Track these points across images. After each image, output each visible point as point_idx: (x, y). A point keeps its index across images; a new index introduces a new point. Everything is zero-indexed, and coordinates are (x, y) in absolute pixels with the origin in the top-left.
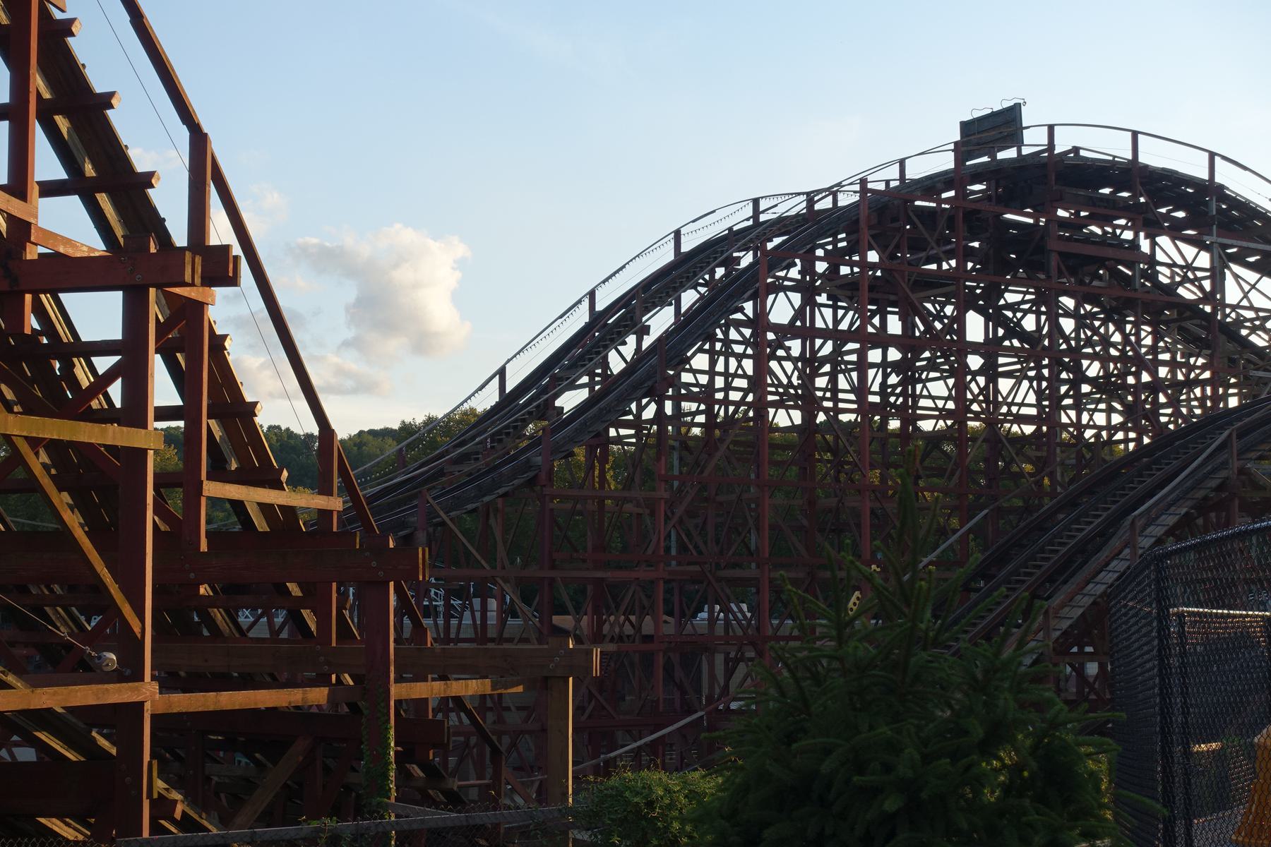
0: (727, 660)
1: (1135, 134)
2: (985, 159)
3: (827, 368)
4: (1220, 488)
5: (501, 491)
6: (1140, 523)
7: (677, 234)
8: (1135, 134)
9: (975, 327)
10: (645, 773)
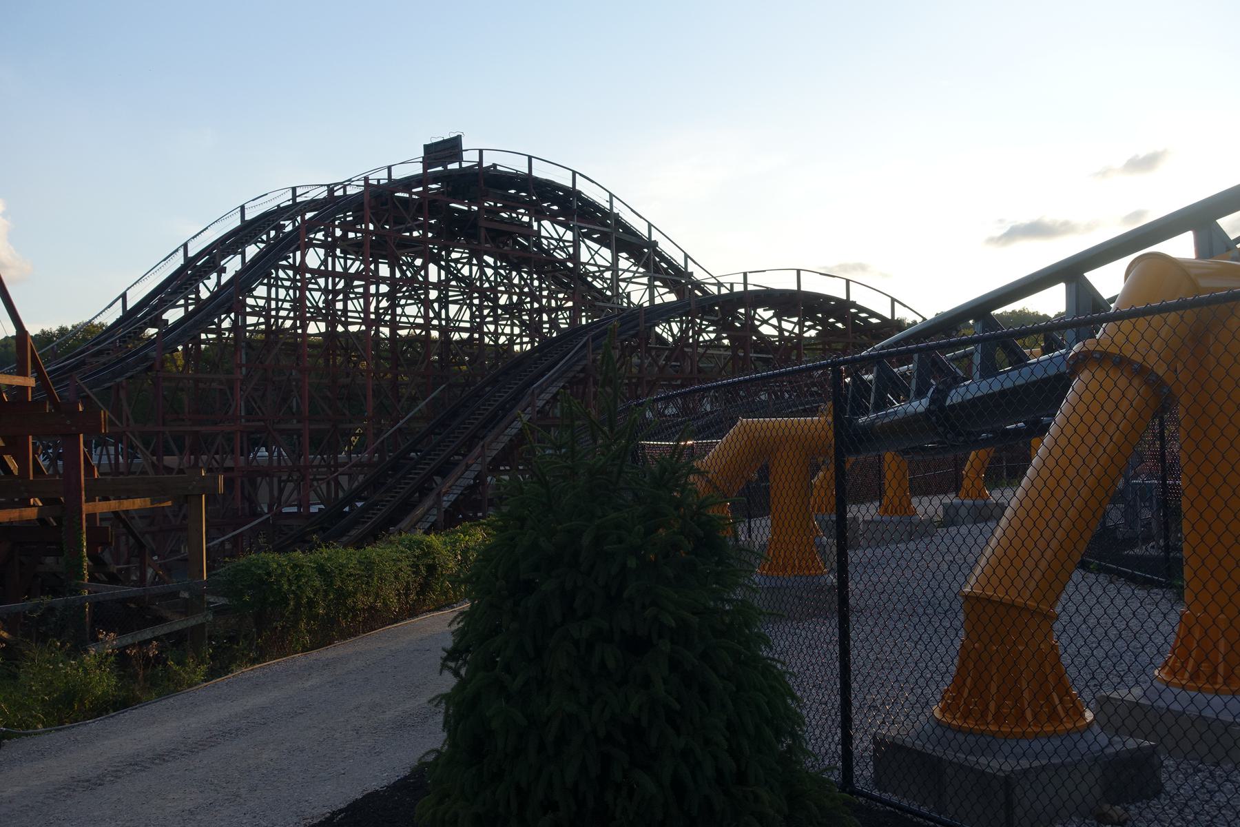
0: (280, 482)
1: (530, 158)
2: (440, 168)
3: (341, 297)
4: (582, 371)
5: (128, 374)
6: (536, 392)
7: (243, 208)
8: (530, 158)
9: (433, 273)
10: (263, 554)
